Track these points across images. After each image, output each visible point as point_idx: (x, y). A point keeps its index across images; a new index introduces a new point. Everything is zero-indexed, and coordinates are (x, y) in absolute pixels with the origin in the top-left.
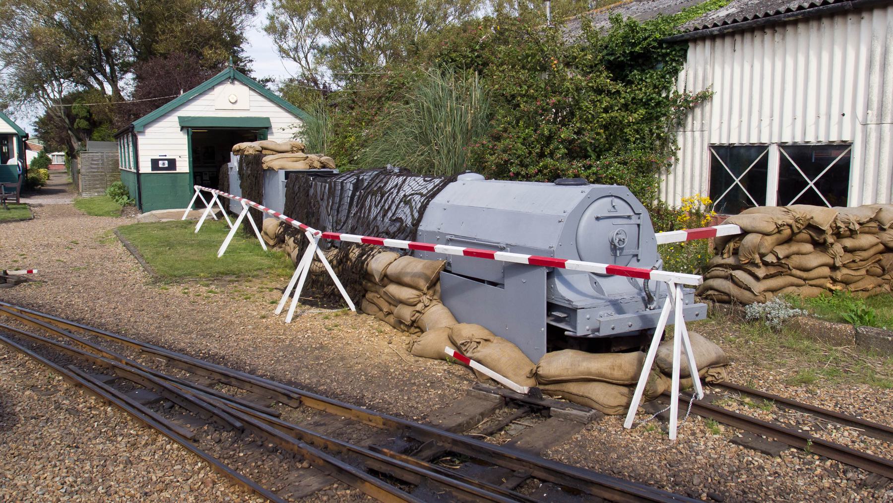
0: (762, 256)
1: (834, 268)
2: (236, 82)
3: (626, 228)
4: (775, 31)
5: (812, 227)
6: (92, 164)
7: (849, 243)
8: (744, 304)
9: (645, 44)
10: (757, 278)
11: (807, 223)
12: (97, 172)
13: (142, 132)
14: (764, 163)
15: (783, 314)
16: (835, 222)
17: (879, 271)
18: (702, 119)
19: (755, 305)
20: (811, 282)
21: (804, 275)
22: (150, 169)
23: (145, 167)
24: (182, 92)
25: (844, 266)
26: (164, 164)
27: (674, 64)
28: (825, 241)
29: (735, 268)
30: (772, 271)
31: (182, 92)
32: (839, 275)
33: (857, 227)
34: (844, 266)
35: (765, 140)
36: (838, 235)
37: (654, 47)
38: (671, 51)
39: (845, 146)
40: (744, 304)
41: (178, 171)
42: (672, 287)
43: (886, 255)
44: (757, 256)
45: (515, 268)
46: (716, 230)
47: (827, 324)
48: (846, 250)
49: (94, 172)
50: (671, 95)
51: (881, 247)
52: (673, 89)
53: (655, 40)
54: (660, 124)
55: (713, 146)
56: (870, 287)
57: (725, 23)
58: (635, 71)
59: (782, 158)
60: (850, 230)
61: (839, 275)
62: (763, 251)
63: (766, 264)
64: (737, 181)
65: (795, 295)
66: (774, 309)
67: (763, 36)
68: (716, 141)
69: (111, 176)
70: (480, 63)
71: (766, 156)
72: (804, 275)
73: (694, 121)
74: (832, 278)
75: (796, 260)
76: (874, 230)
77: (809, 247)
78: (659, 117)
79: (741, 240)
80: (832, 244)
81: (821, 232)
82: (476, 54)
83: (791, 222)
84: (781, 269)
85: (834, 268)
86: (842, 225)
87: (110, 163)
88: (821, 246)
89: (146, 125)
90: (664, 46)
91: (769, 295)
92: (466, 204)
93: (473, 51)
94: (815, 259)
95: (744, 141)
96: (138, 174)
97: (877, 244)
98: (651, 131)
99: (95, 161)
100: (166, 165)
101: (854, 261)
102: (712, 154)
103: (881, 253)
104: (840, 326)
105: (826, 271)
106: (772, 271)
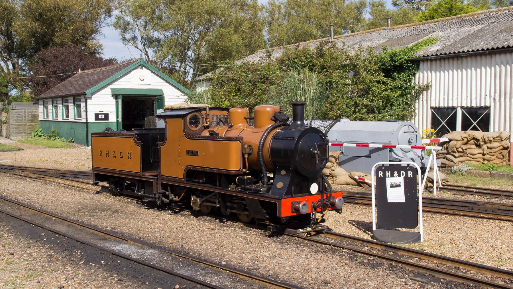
0: (457, 149)
1: (484, 154)
2: (144, 68)
3: (413, 136)
4: (458, 60)
5: (475, 139)
6: (18, 117)
7: (489, 145)
8: (451, 167)
9: (400, 61)
10: (455, 157)
11: (472, 137)
12: (21, 122)
13: (90, 98)
14: (455, 115)
15: (465, 169)
16: (483, 137)
17: (501, 157)
18: (427, 96)
19: (455, 167)
20: (475, 160)
21: (473, 157)
22: (94, 119)
23: (91, 119)
24: (80, 70)
25: (488, 154)
26: (102, 116)
27: (414, 71)
28: (480, 144)
29: (447, 154)
30: (461, 154)
31: (80, 70)
32: (486, 157)
33: (492, 139)
34: (488, 154)
35: (455, 105)
36: (485, 142)
37: (405, 63)
38: (412, 65)
39: (488, 108)
40: (451, 167)
41: (110, 121)
42: (433, 150)
43: (504, 151)
44: (455, 149)
45: (378, 150)
46: (439, 140)
47: (481, 171)
48: (488, 148)
49: (19, 122)
50: (412, 85)
51: (502, 147)
52: (413, 81)
53: (405, 60)
54: (408, 97)
55: (432, 108)
56: (498, 163)
57: (437, 55)
58: (396, 73)
59: (463, 113)
60: (490, 140)
61: (486, 157)
62: (457, 147)
63: (458, 152)
64: (443, 123)
65: (469, 163)
66: (462, 167)
67: (453, 61)
68: (433, 105)
69: (30, 125)
70: (311, 65)
71: (456, 112)
72: (473, 157)
73: (424, 96)
74: (483, 159)
75: (469, 151)
76: (499, 141)
77: (474, 146)
78: (407, 94)
79: (449, 144)
80: (482, 145)
81: (478, 140)
82: (309, 60)
83: (467, 136)
84: (464, 154)
85: (484, 154)
86: (486, 138)
87: (30, 116)
88: (479, 146)
89: (93, 94)
90: (409, 62)
91: (460, 163)
92: (349, 129)
93: (306, 58)
94: (476, 151)
95: (446, 106)
96: (87, 123)
97: (500, 146)
98: (403, 101)
99: (20, 115)
100: (103, 117)
101: (491, 152)
102: (432, 112)
103: (502, 150)
104: (485, 171)
105: (481, 155)
106: (461, 154)
